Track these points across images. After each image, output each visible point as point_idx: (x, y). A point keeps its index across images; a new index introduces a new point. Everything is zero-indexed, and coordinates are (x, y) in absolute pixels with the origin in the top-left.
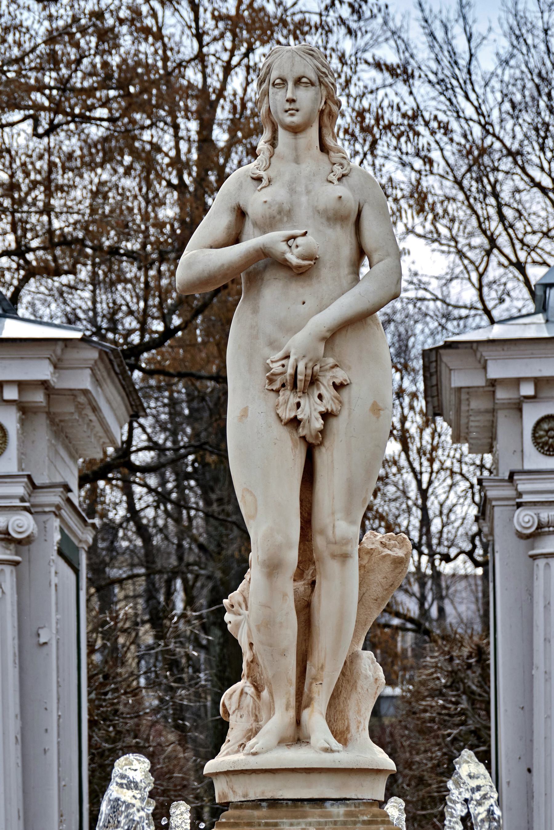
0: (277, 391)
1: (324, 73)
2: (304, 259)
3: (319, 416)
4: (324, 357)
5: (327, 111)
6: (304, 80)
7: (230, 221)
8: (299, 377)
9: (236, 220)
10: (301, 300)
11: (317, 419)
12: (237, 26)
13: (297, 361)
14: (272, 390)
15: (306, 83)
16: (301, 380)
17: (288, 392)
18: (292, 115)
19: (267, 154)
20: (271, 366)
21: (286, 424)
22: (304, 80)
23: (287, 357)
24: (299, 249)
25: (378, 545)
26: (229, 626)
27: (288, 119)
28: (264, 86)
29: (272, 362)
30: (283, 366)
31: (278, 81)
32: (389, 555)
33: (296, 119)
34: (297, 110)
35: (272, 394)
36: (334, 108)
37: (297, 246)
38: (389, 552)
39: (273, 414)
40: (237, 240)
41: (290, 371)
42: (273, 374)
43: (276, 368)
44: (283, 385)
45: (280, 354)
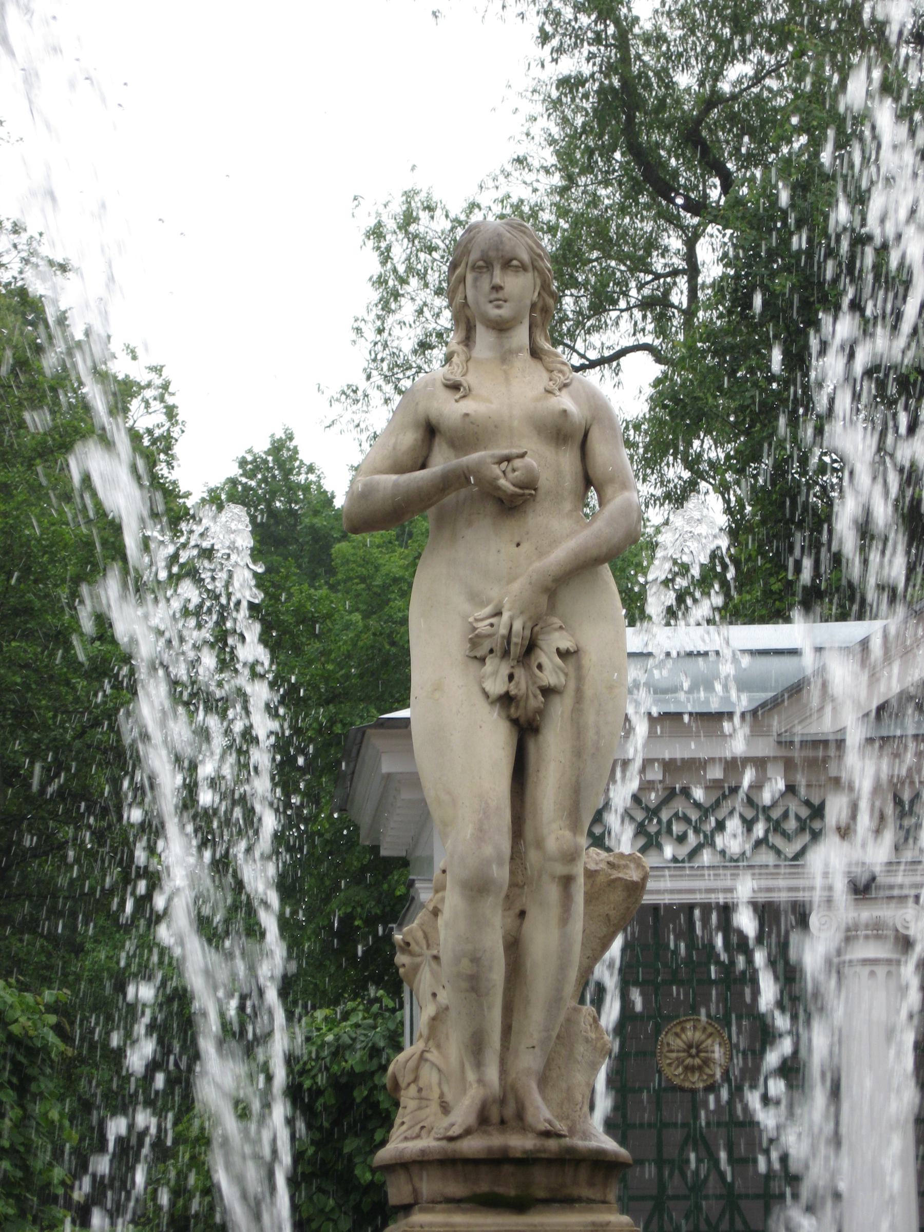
0: (482, 660)
1: (539, 256)
2: (521, 488)
3: (538, 692)
4: (547, 615)
5: (540, 305)
6: (515, 262)
7: (416, 440)
8: (514, 640)
9: (423, 441)
10: (517, 540)
11: (535, 696)
12: (828, 12)
13: (512, 619)
14: (476, 657)
15: (516, 267)
16: (516, 644)
17: (497, 660)
18: (499, 307)
19: (463, 357)
20: (475, 625)
21: (492, 703)
22: (515, 262)
23: (498, 614)
24: (516, 473)
25: (603, 866)
26: (401, 970)
27: (494, 312)
28: (459, 271)
29: (477, 620)
30: (492, 625)
31: (481, 263)
32: (620, 879)
33: (505, 312)
34: (505, 301)
35: (476, 664)
36: (551, 302)
37: (514, 470)
38: (621, 875)
39: (476, 690)
40: (423, 466)
41: (503, 631)
42: (477, 636)
43: (483, 627)
44: (491, 651)
45: (488, 610)
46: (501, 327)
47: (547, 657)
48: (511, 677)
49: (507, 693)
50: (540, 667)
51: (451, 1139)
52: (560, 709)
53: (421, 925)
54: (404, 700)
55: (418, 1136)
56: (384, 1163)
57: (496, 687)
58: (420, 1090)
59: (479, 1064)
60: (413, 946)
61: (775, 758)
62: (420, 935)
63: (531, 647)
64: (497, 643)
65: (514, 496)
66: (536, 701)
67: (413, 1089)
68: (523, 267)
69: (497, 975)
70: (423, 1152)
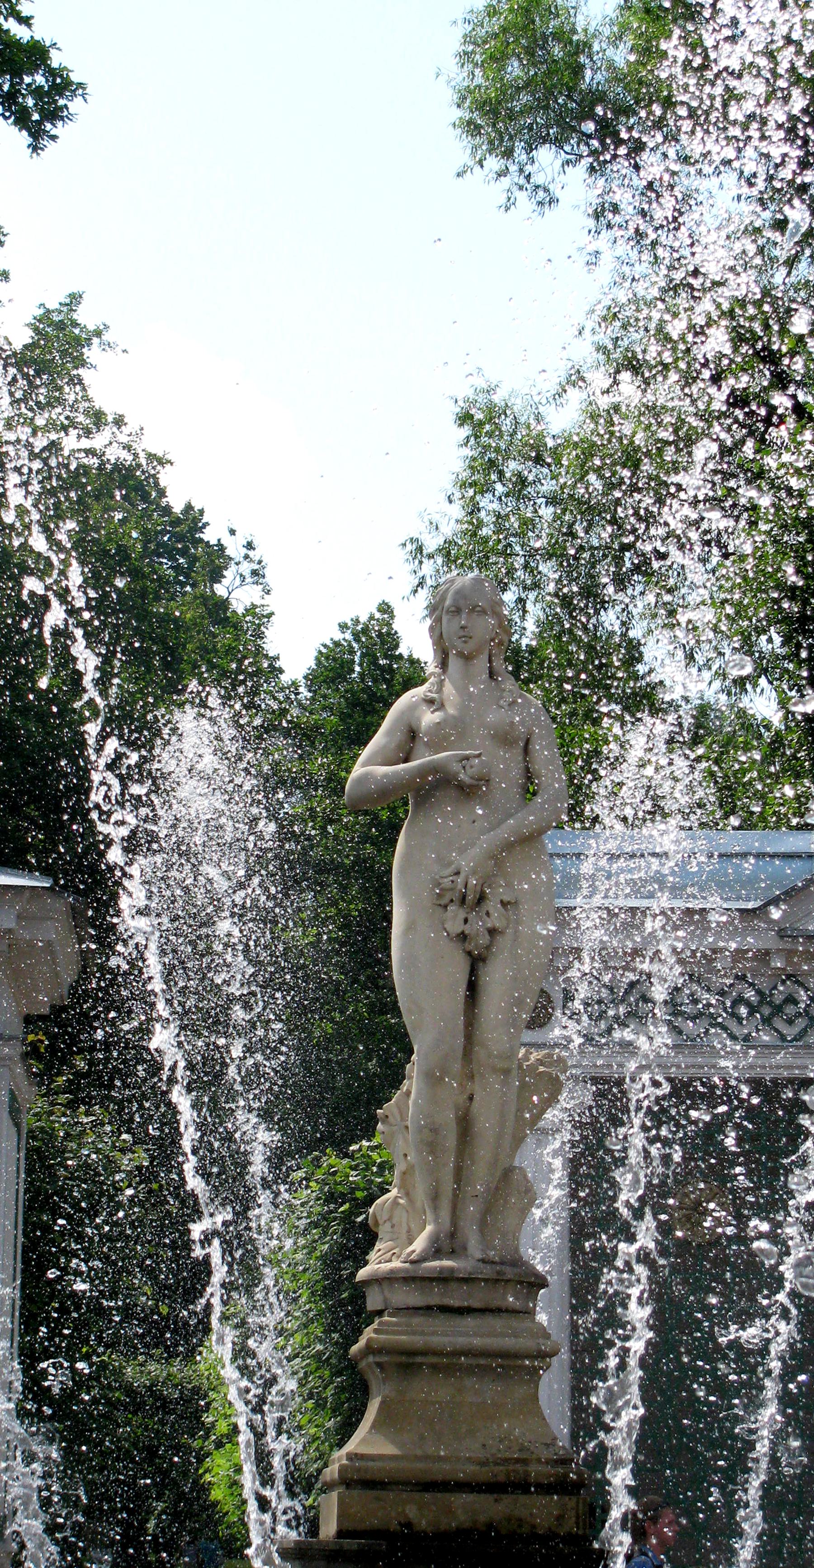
0: (445, 907)
13: (467, 878)
35: (440, 910)
40: (406, 760)
41: (460, 886)
43: (446, 883)
46: (467, 658)
47: (492, 905)
48: (466, 921)
49: (463, 933)
50: (488, 914)
51: (412, 1262)
52: (504, 942)
53: (397, 1103)
54: (450, 626)
55: (390, 1261)
56: (368, 1477)
57: (456, 927)
58: (393, 1226)
59: (436, 1208)
60: (391, 1119)
61: (779, 950)
62: (395, 1111)
63: (481, 899)
64: (456, 896)
65: (471, 786)
66: (484, 940)
67: (388, 1225)
68: (484, 612)
69: (451, 1141)
70: (392, 1271)
